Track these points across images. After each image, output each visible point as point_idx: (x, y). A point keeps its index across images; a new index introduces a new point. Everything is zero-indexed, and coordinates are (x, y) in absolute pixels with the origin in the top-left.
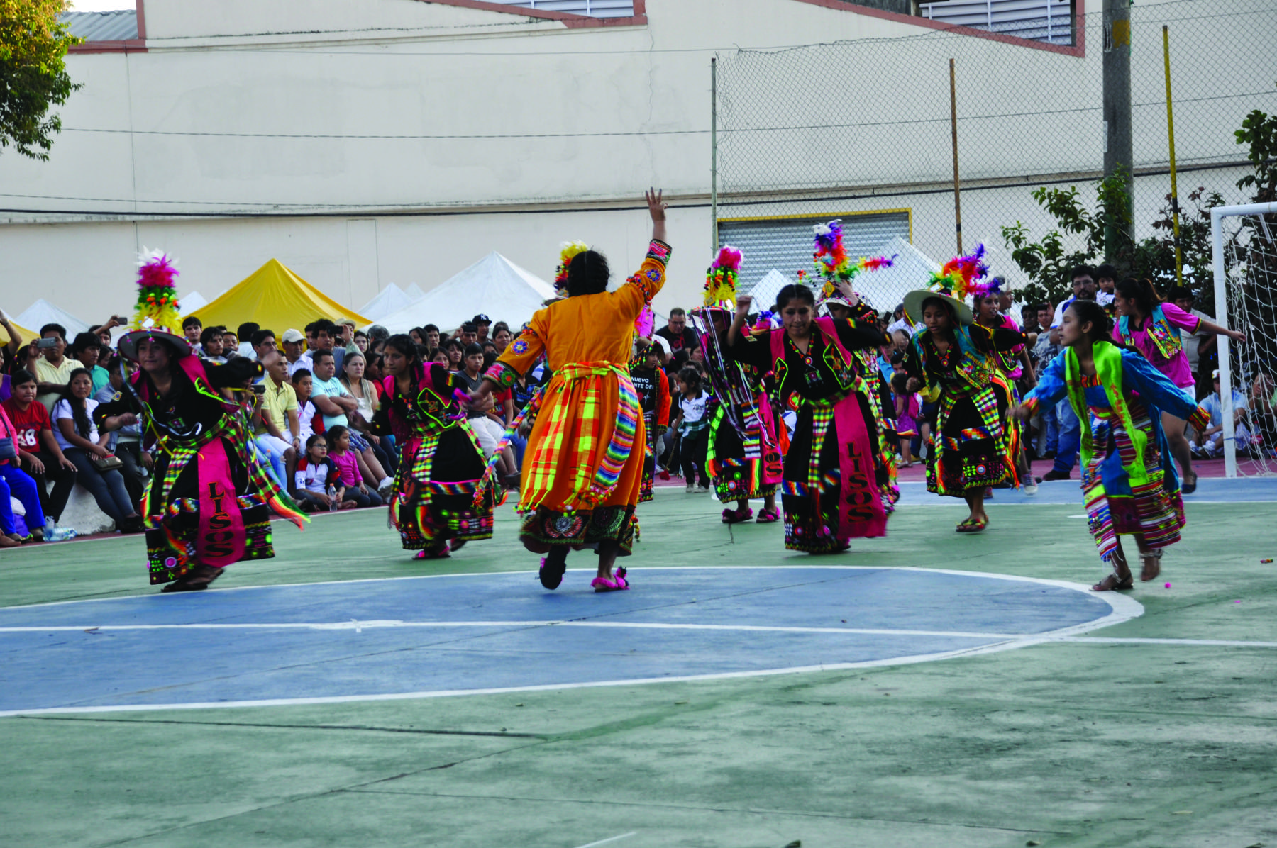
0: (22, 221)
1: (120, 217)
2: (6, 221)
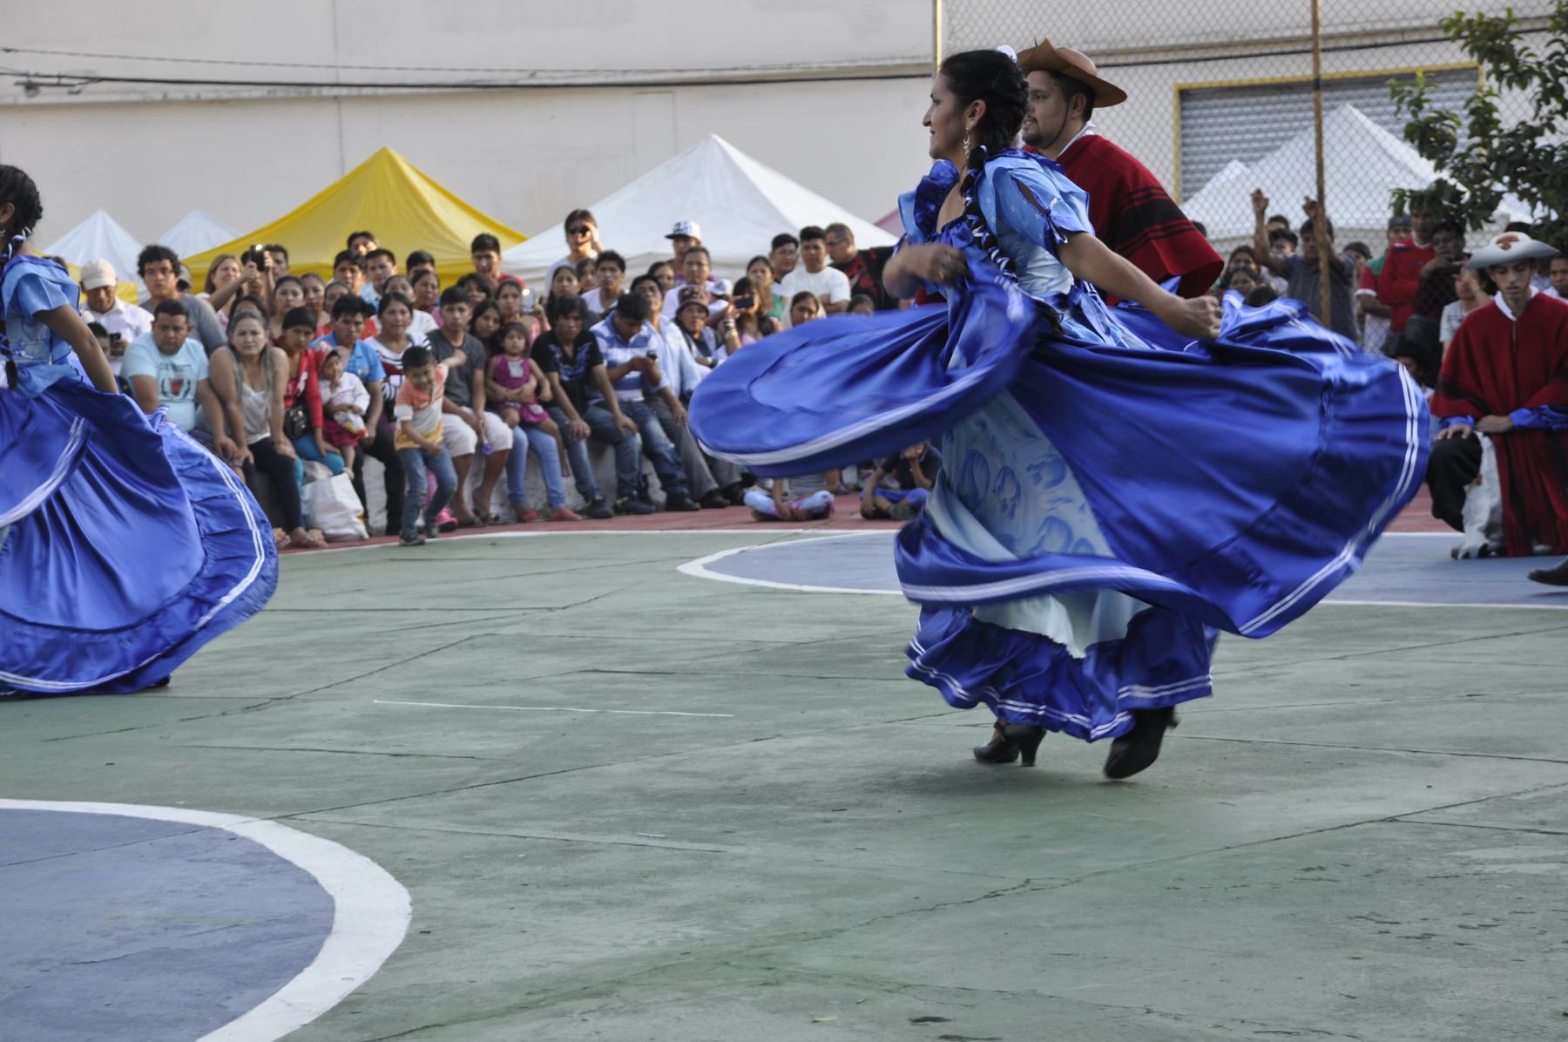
0: (180, 96)
1: (314, 91)
2: (159, 97)
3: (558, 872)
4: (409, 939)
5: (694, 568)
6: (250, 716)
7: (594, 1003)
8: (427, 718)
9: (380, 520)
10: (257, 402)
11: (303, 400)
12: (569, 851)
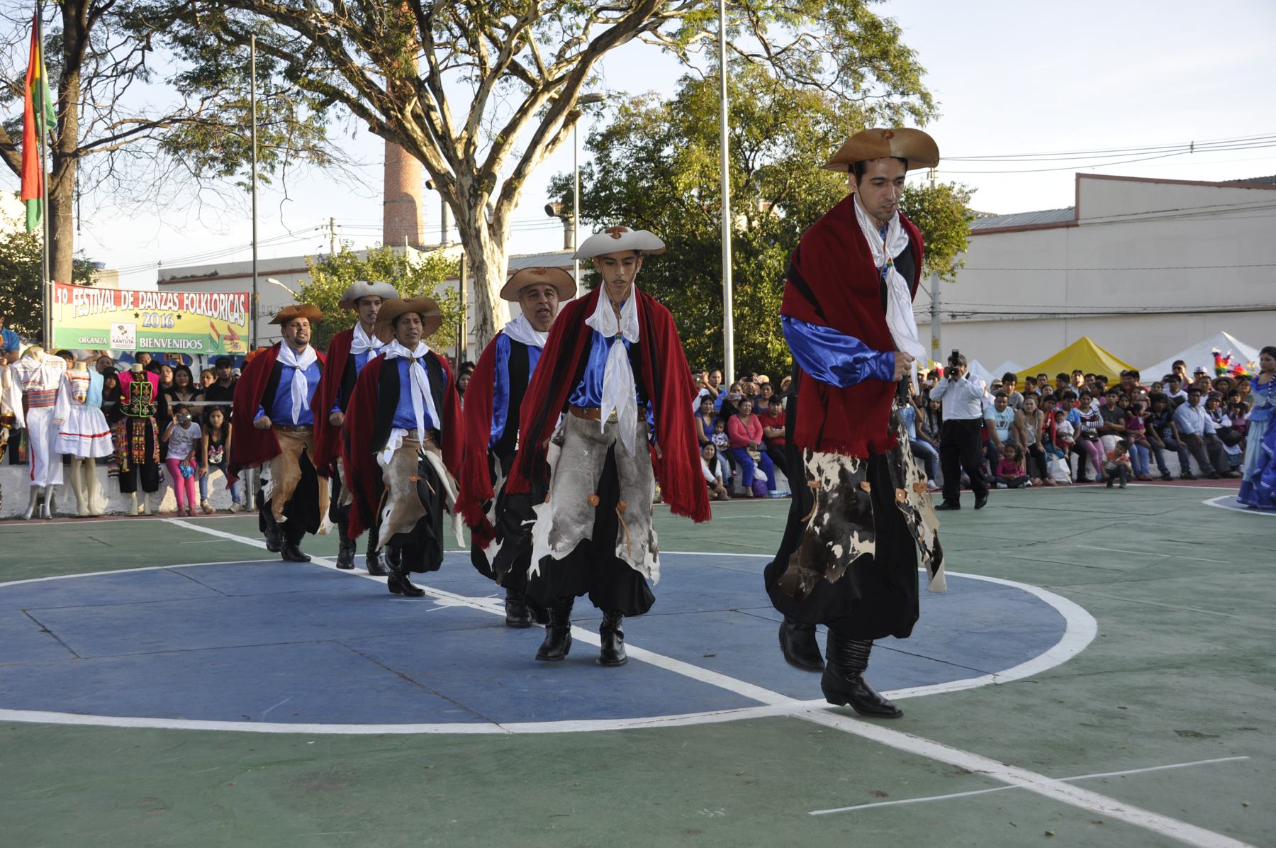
3: (1157, 618)
4: (1097, 638)
5: (1210, 502)
6: (1030, 548)
7: (1176, 671)
8: (1100, 554)
9: (1075, 476)
10: (1031, 432)
11: (1049, 430)
12: (1161, 610)
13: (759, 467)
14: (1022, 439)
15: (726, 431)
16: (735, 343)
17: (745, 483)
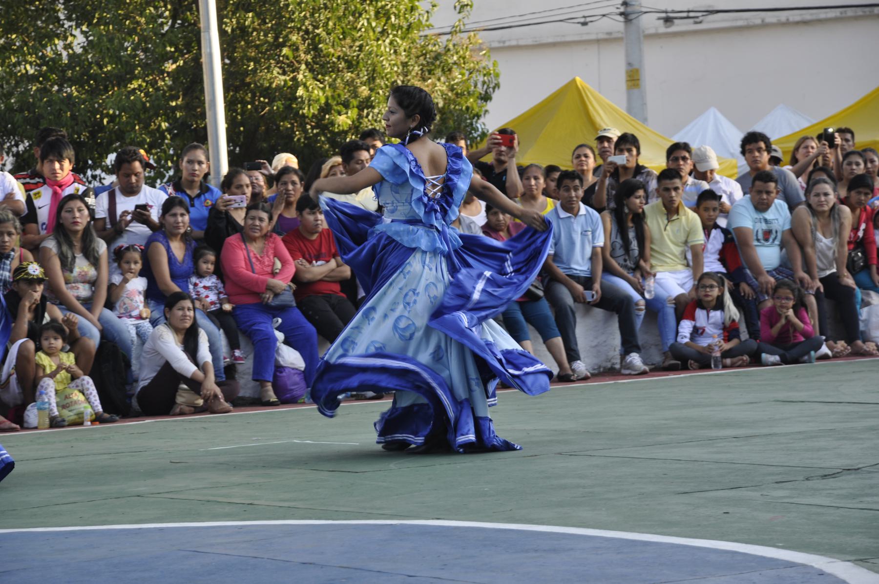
6: (831, 482)
13: (286, 342)
14: (808, 267)
15: (219, 272)
16: (227, 89)
17: (258, 377)
